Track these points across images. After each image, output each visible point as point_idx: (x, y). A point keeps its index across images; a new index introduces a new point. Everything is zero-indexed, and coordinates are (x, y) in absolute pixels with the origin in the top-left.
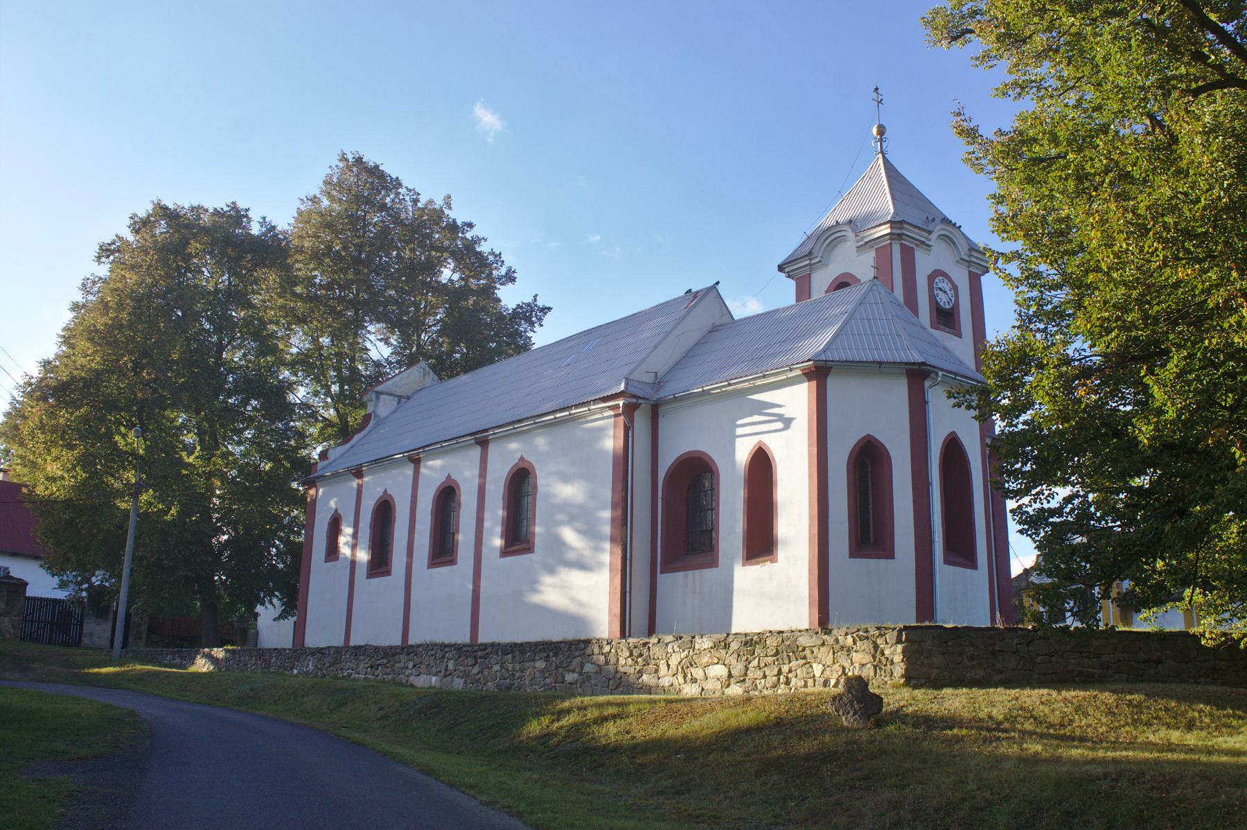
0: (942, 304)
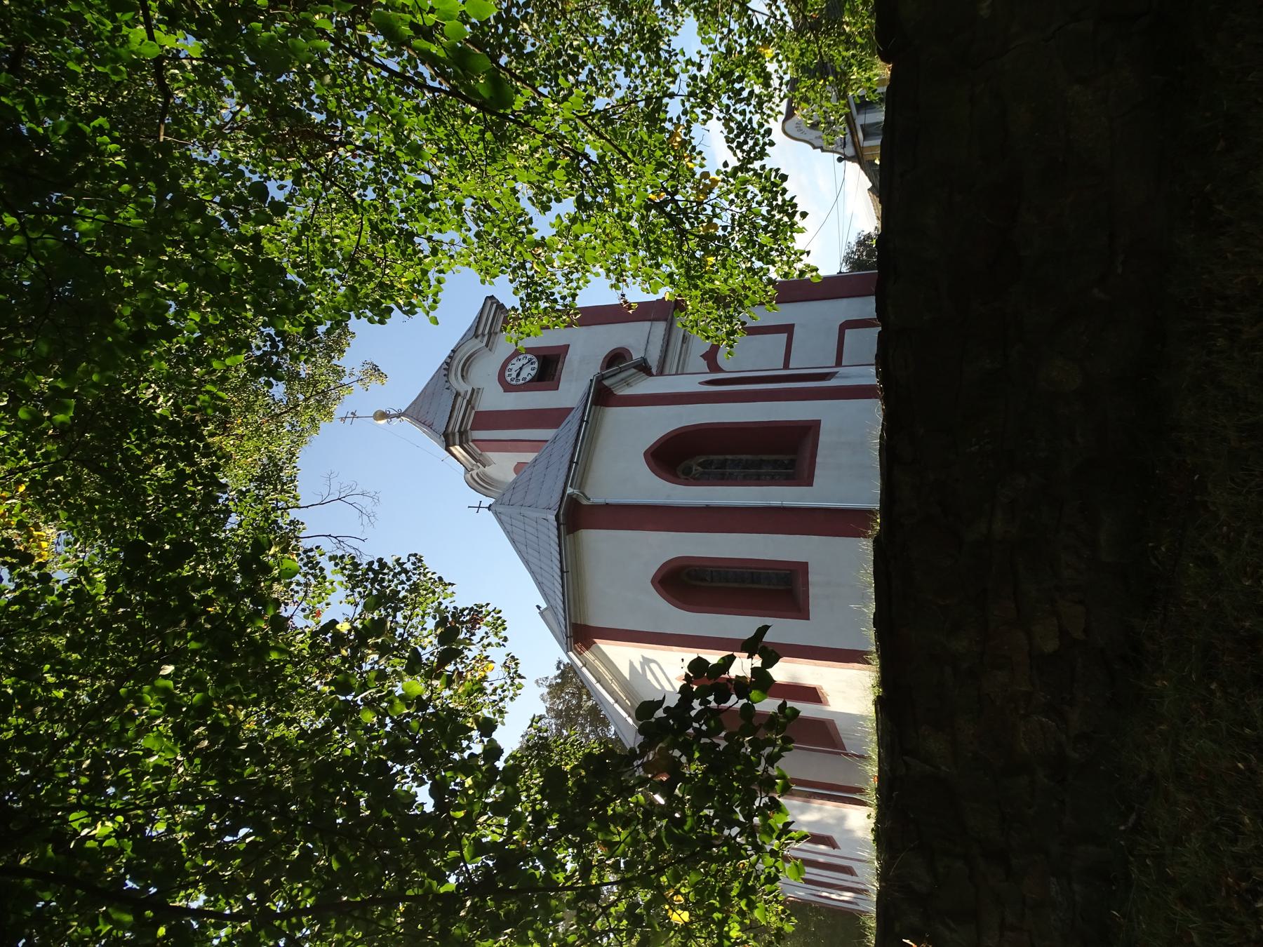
0: (533, 373)
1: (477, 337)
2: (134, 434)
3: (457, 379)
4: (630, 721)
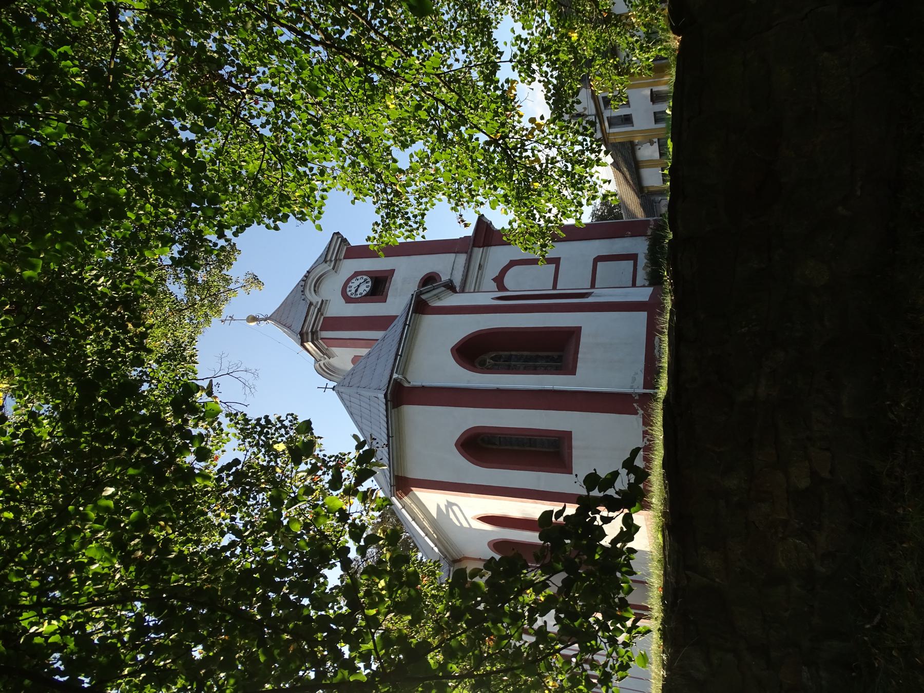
0: (368, 289)
1: (326, 262)
2: (79, 307)
3: (310, 293)
4: (436, 549)
